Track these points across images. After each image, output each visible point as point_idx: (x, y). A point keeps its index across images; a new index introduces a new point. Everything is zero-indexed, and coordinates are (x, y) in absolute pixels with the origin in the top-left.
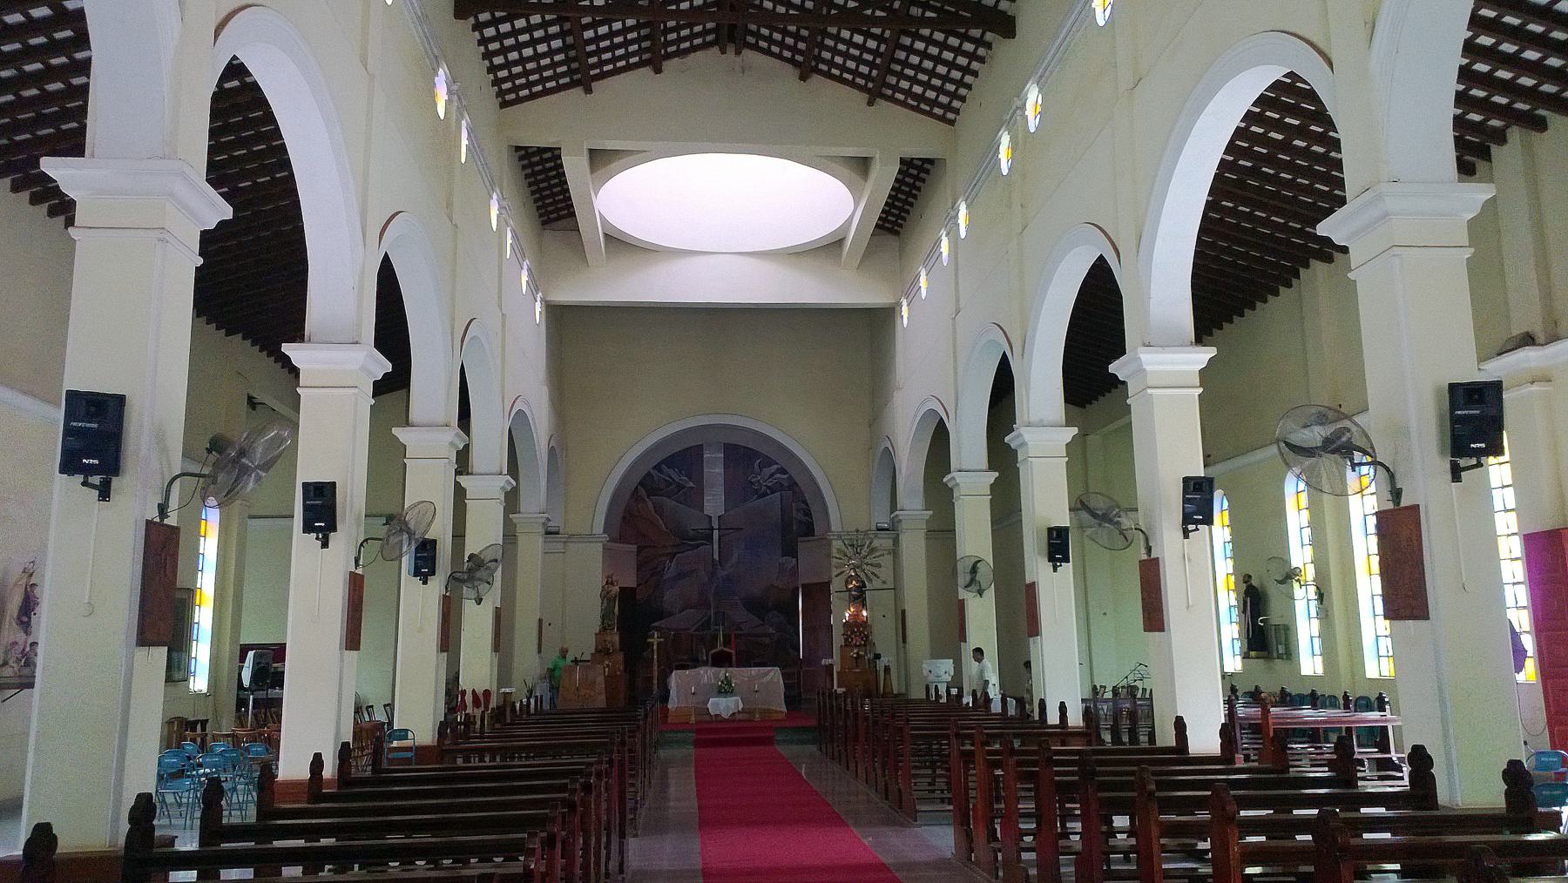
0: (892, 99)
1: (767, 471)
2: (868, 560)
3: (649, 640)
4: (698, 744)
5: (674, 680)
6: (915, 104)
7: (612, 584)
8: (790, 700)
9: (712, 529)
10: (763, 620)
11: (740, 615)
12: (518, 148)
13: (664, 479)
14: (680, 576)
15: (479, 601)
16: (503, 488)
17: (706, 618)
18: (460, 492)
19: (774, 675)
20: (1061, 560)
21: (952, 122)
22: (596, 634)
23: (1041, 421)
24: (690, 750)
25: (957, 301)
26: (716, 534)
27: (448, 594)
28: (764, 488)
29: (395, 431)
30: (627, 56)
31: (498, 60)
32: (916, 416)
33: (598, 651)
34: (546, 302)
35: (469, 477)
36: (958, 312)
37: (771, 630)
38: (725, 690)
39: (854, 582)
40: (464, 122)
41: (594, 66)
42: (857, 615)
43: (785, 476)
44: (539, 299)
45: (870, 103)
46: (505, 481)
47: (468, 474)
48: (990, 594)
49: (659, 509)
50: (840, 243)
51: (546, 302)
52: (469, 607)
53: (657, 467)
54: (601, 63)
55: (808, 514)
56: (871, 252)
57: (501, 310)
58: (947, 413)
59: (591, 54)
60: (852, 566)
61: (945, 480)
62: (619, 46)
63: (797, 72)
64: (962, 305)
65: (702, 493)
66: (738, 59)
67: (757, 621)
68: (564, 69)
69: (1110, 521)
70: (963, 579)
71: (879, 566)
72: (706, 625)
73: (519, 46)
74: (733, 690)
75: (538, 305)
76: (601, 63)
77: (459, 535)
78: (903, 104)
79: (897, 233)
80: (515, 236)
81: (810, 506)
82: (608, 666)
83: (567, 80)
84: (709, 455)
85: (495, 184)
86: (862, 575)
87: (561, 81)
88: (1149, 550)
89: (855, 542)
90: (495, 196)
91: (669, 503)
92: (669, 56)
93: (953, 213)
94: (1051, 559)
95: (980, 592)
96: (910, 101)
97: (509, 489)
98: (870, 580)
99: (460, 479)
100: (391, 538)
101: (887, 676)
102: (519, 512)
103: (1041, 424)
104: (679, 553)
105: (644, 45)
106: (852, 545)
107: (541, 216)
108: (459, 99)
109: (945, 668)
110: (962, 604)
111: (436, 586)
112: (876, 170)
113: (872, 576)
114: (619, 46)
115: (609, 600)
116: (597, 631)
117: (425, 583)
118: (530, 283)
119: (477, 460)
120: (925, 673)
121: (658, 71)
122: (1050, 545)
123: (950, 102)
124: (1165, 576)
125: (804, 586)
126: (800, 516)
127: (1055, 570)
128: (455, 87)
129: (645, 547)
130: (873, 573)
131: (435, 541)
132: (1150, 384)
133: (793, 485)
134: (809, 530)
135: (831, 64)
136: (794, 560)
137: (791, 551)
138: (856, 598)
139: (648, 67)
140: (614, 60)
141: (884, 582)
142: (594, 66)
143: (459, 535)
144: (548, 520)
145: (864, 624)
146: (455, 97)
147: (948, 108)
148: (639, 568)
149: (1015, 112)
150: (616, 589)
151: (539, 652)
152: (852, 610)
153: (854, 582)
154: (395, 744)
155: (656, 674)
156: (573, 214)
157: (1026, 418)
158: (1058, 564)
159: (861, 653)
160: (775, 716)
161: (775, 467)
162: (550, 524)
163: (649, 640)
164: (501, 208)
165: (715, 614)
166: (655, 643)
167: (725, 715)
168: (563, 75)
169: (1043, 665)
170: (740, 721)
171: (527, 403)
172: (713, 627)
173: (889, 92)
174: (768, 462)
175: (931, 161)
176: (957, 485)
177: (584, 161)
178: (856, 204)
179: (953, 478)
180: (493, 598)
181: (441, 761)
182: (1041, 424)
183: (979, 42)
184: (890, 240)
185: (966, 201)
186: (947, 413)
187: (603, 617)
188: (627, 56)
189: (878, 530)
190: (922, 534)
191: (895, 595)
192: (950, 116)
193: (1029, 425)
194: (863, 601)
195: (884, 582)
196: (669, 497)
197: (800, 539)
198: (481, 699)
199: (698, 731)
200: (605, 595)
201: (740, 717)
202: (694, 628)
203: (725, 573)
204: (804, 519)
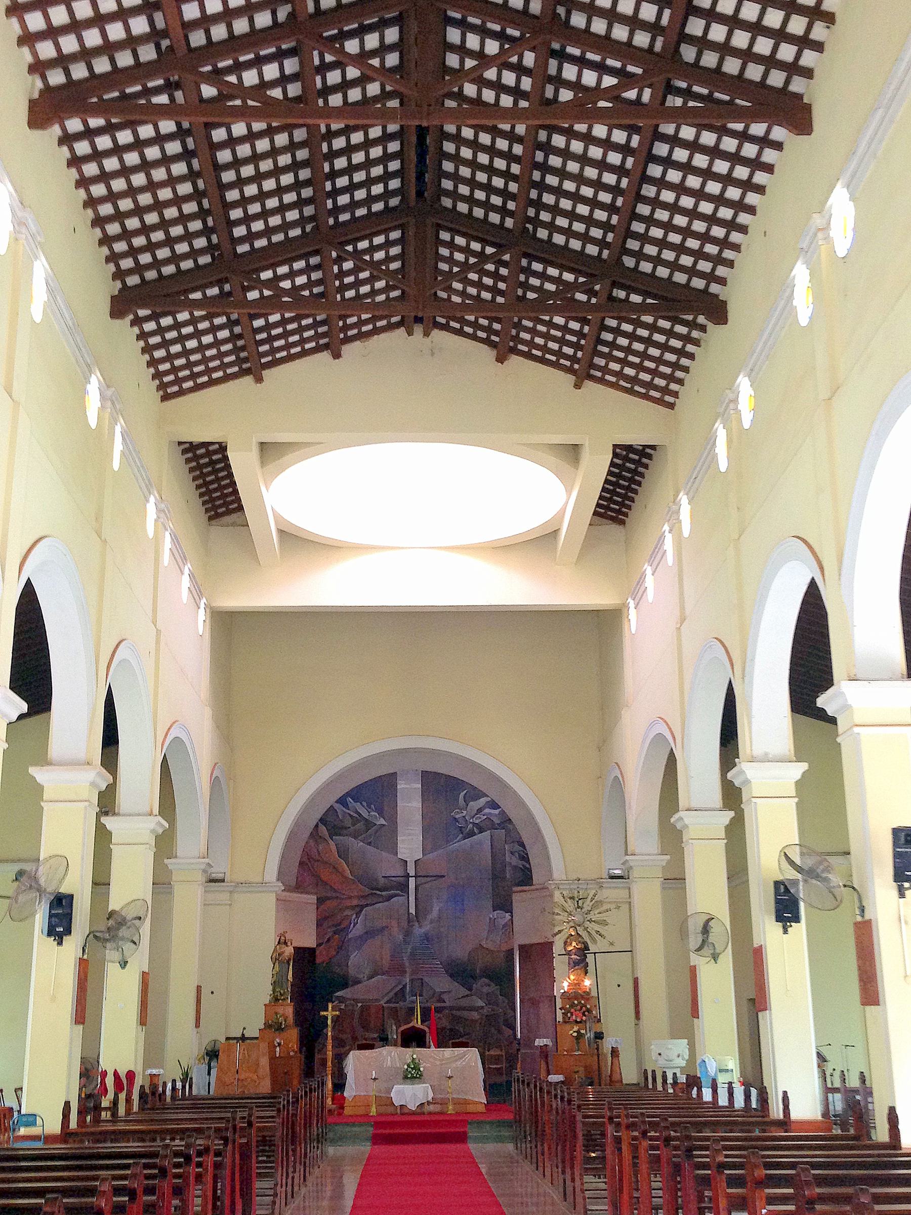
0: (601, 381)
1: (475, 805)
2: (594, 916)
3: (322, 1013)
4: (377, 1140)
5: (355, 1061)
6: (629, 386)
7: (285, 943)
8: (491, 1088)
9: (408, 876)
10: (470, 990)
11: (441, 983)
12: (180, 443)
13: (351, 816)
14: (370, 934)
15: (124, 964)
16: (153, 831)
17: (401, 987)
18: (103, 837)
19: (471, 1057)
20: (790, 920)
21: (671, 406)
22: (265, 1005)
23: (766, 754)
24: (366, 1148)
25: (682, 608)
26: (412, 882)
27: (85, 957)
28: (471, 825)
29: (33, 771)
30: (303, 341)
31: (159, 354)
32: (643, 742)
33: (268, 1026)
34: (211, 608)
35: (115, 818)
36: (683, 620)
37: (480, 1003)
38: (413, 1074)
39: (574, 944)
40: (118, 429)
41: (265, 354)
42: (577, 984)
43: (497, 812)
44: (202, 606)
45: (578, 386)
46: (157, 823)
47: (114, 814)
48: (727, 959)
49: (343, 853)
50: (556, 532)
51: (211, 608)
52: (112, 970)
53: (342, 801)
54: (273, 351)
55: (525, 858)
56: (589, 544)
57: (155, 626)
58: (674, 738)
59: (262, 342)
60: (572, 924)
61: (672, 820)
62: (293, 333)
63: (494, 353)
64: (687, 612)
65: (394, 832)
66: (427, 340)
67: (463, 991)
68: (233, 358)
69: (817, 877)
70: (694, 940)
71: (604, 923)
72: (401, 994)
73: (182, 339)
74: (421, 1075)
75: (202, 611)
76: (273, 351)
77: (101, 883)
78: (614, 386)
79: (622, 523)
80: (175, 539)
81: (527, 848)
82: (279, 1044)
83: (236, 369)
84: (403, 786)
85: (151, 485)
86: (584, 934)
87: (229, 371)
88: (862, 909)
89: (576, 895)
90: (152, 499)
91: (356, 845)
92: (348, 340)
93: (674, 507)
94: (779, 918)
95: (715, 957)
96: (622, 383)
97: (160, 831)
98: (594, 941)
99: (104, 820)
100: (20, 897)
101: (615, 1061)
102: (176, 857)
103: (766, 759)
104: (367, 905)
105: (320, 330)
106: (572, 898)
107: (207, 511)
108: (113, 403)
109: (681, 1046)
110: (693, 971)
111: (73, 945)
112: (586, 456)
113: (598, 937)
114: (293, 333)
115: (281, 962)
116: (267, 1002)
117: (60, 943)
118: (192, 589)
119: (124, 798)
120: (654, 1056)
121: (337, 355)
122: (778, 902)
123: (668, 385)
124: (879, 941)
125: (522, 948)
126: (515, 861)
127: (785, 931)
128: (109, 393)
129: (328, 898)
130: (597, 932)
131: (72, 896)
132: (857, 722)
133: (506, 821)
134: (525, 877)
135: (531, 344)
136: (508, 915)
137: (504, 905)
138: (576, 963)
139: (325, 352)
140: (288, 346)
141: (612, 944)
142: (265, 354)
143: (101, 883)
144: (209, 864)
145: (586, 995)
146: (109, 404)
147: (665, 391)
148: (319, 925)
149: (727, 406)
150: (289, 951)
151: (197, 1025)
152: (572, 977)
153: (574, 944)
154: (23, 1131)
155: (330, 1054)
156: (240, 508)
157: (748, 751)
158: (788, 924)
159: (583, 1032)
160: (471, 1108)
161: (483, 801)
162: (210, 871)
163: (322, 1013)
164: (159, 510)
165: (412, 980)
166: (330, 1018)
167: (412, 1107)
168: (231, 364)
169: (773, 1045)
170: (430, 1113)
171: (184, 728)
172: (409, 998)
173: (599, 374)
174: (476, 794)
175: (653, 447)
176: (686, 826)
177: (254, 454)
178: (569, 492)
179: (681, 819)
180: (139, 961)
181: (66, 1142)
182: (766, 759)
183: (693, 325)
184: (613, 529)
185: (687, 494)
186: (674, 738)
187: (274, 984)
188: (303, 341)
189: (612, 877)
190: (657, 885)
191: (632, 957)
192: (668, 398)
193: (753, 760)
194: (585, 968)
195: (612, 944)
196: (355, 838)
197: (515, 889)
198: (125, 1081)
199: (377, 1125)
200: (277, 958)
201: (432, 1108)
202: (386, 999)
203: (423, 930)
204: (520, 863)
